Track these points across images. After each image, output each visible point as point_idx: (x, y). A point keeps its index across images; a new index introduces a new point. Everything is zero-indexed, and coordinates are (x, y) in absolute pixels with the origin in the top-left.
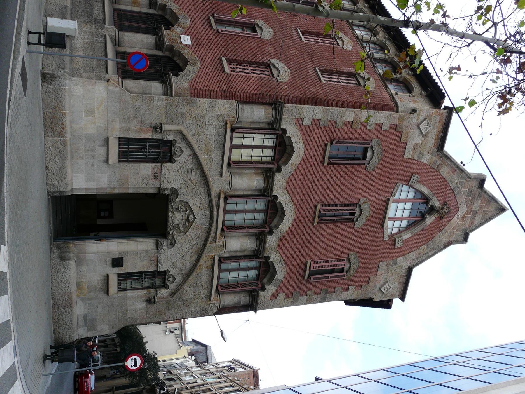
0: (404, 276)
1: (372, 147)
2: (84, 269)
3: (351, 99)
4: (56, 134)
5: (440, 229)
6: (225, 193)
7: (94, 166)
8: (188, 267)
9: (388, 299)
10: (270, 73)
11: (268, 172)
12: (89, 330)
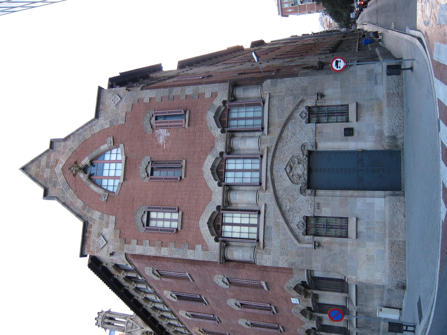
0: (102, 110)
1: (143, 225)
2: (376, 127)
3: (164, 263)
4: (397, 244)
5: (75, 152)
6: (261, 189)
7: (368, 216)
8: (290, 126)
9: (113, 89)
10: (229, 279)
11: (227, 206)
12: (373, 70)
